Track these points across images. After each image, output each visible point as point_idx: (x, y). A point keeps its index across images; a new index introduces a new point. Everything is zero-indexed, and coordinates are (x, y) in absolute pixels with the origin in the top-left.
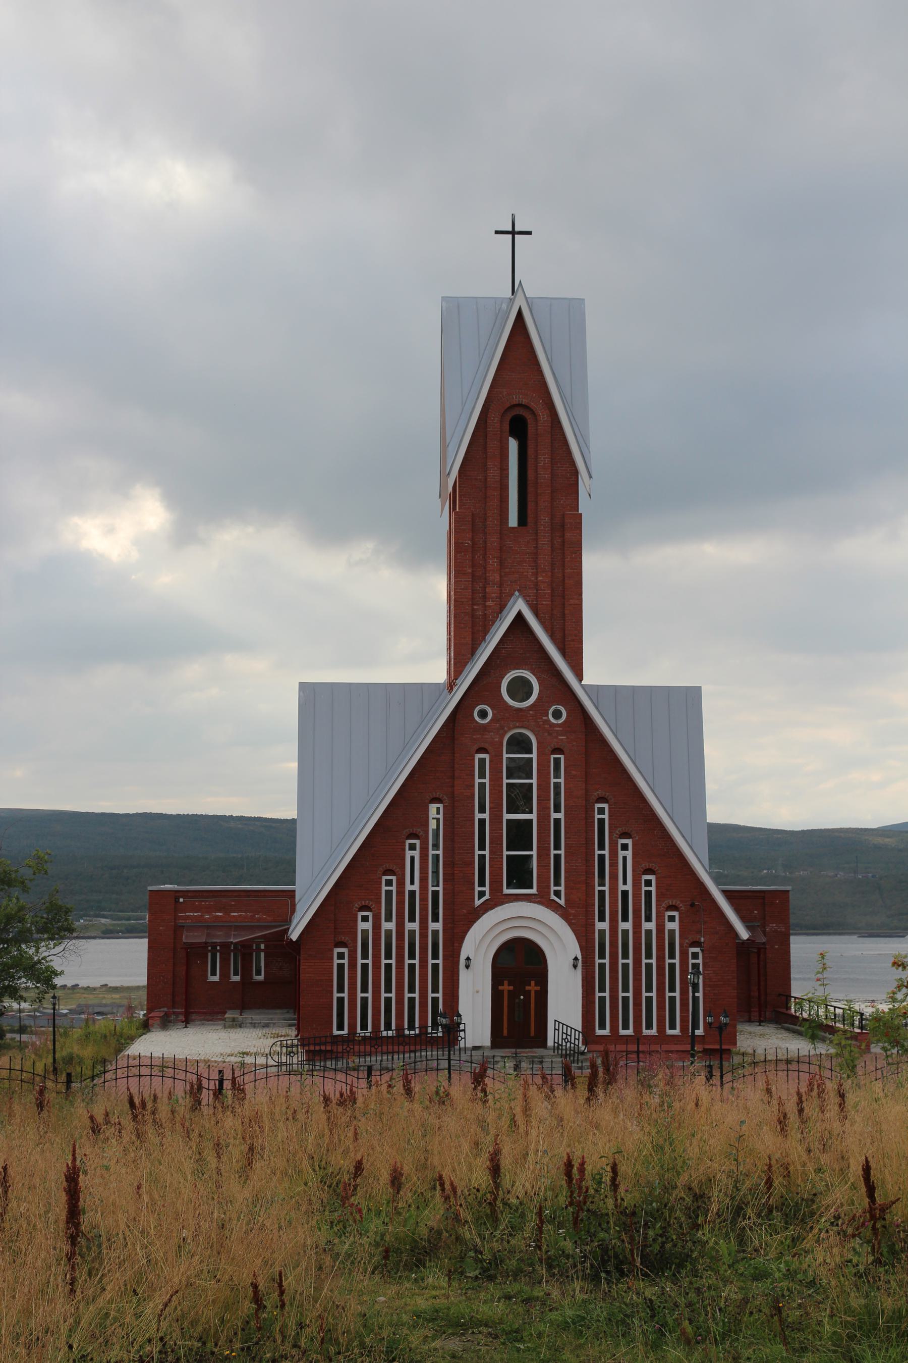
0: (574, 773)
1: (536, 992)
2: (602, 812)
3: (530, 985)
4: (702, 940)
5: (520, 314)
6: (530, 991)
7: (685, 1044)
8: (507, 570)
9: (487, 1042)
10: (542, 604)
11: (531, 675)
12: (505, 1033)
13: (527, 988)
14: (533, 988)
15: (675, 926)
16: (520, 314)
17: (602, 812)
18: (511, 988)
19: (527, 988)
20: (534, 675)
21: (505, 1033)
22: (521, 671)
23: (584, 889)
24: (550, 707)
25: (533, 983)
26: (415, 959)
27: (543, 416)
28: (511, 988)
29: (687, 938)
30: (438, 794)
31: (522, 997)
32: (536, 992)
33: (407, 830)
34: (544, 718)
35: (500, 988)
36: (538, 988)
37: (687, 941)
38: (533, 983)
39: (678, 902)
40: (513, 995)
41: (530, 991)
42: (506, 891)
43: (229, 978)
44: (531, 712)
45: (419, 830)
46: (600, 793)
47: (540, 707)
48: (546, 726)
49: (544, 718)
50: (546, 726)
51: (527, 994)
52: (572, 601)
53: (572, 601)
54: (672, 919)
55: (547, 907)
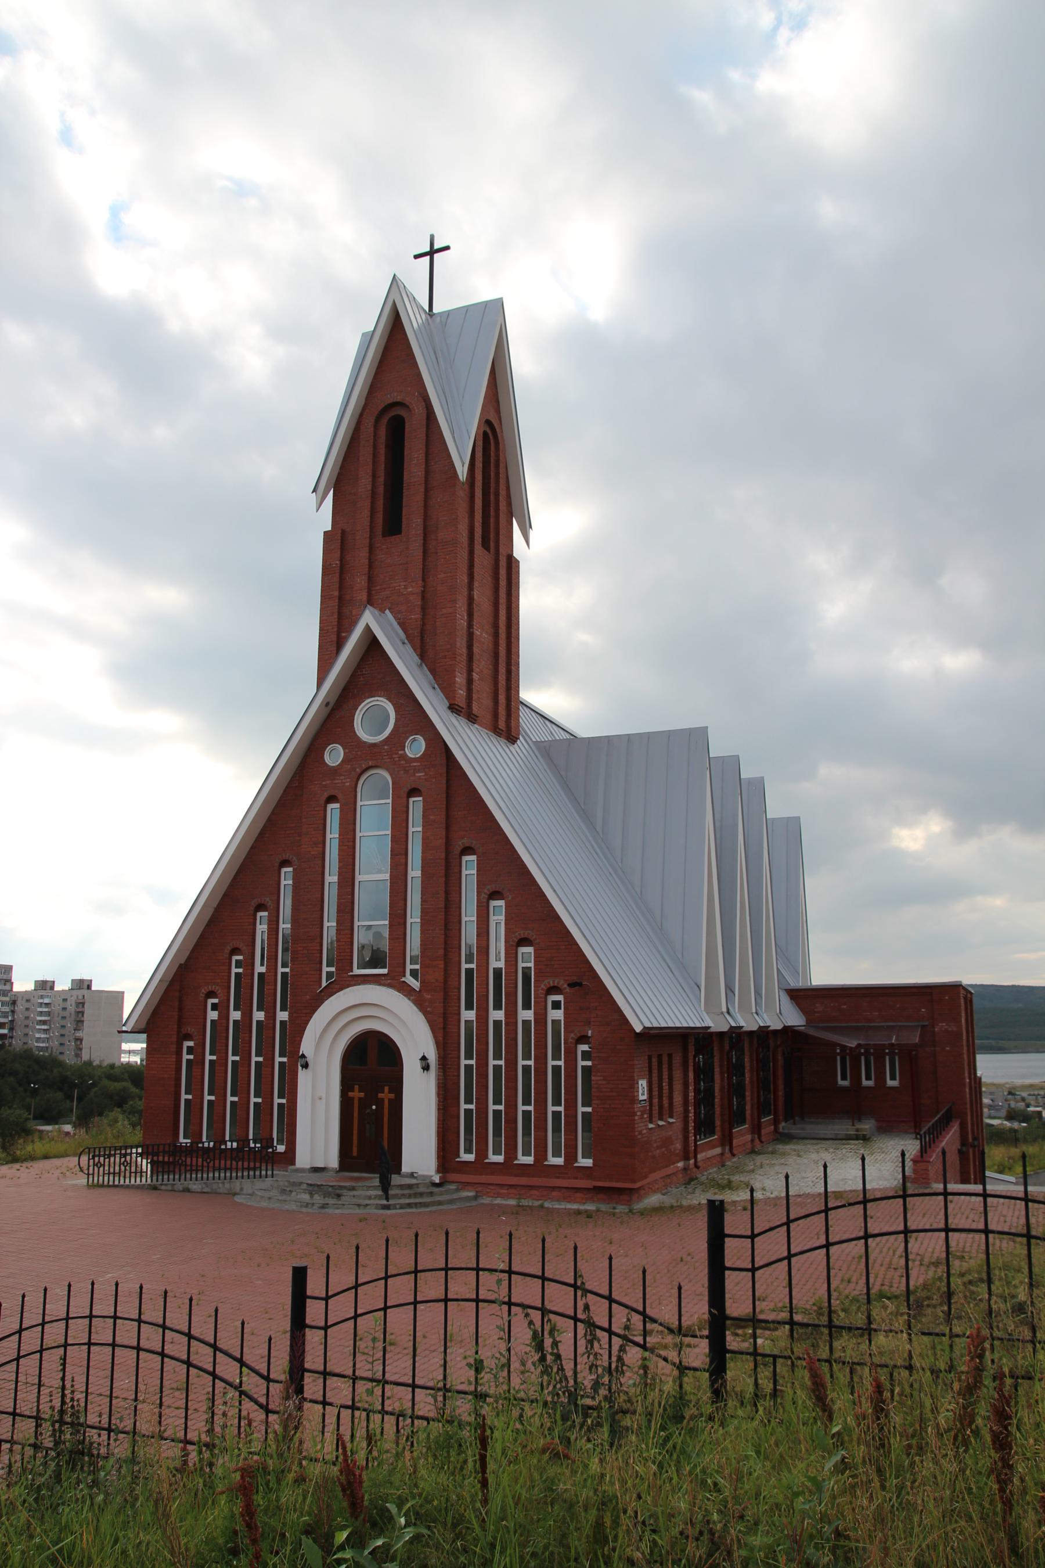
0: (432, 817)
1: (390, 1100)
2: (470, 867)
3: (383, 1092)
4: (590, 1033)
5: (394, 305)
6: (383, 1100)
7: (569, 1178)
8: (378, 588)
9: (334, 1162)
10: (411, 619)
11: (387, 702)
12: (355, 1153)
13: (380, 1095)
14: (386, 1095)
15: (558, 1015)
16: (394, 305)
17: (470, 867)
18: (362, 1095)
19: (380, 1095)
20: (390, 701)
21: (355, 1153)
22: (376, 698)
23: (442, 966)
24: (407, 738)
25: (386, 1089)
26: (523, 1111)
27: (419, 410)
28: (362, 1095)
29: (573, 1032)
30: (287, 856)
31: (374, 1107)
32: (390, 1100)
33: (256, 900)
34: (400, 752)
35: (350, 1094)
36: (392, 1096)
37: (572, 1035)
38: (386, 1089)
39: (562, 982)
40: (364, 1104)
41: (383, 1100)
42: (357, 971)
43: (486, 1156)
44: (386, 747)
45: (268, 899)
46: (466, 842)
47: (397, 740)
48: (402, 762)
49: (400, 752)
50: (402, 762)
51: (380, 1103)
52: (444, 611)
53: (444, 611)
54: (556, 1005)
55: (399, 991)
